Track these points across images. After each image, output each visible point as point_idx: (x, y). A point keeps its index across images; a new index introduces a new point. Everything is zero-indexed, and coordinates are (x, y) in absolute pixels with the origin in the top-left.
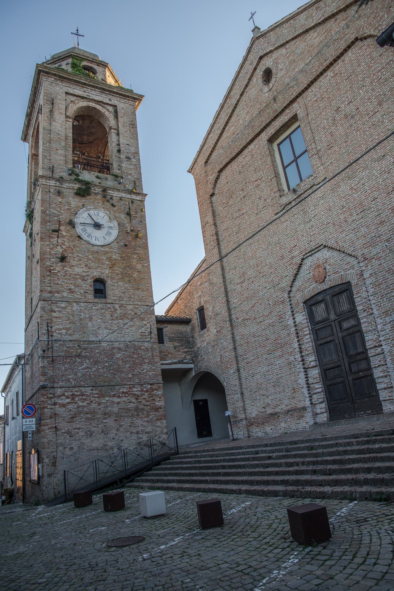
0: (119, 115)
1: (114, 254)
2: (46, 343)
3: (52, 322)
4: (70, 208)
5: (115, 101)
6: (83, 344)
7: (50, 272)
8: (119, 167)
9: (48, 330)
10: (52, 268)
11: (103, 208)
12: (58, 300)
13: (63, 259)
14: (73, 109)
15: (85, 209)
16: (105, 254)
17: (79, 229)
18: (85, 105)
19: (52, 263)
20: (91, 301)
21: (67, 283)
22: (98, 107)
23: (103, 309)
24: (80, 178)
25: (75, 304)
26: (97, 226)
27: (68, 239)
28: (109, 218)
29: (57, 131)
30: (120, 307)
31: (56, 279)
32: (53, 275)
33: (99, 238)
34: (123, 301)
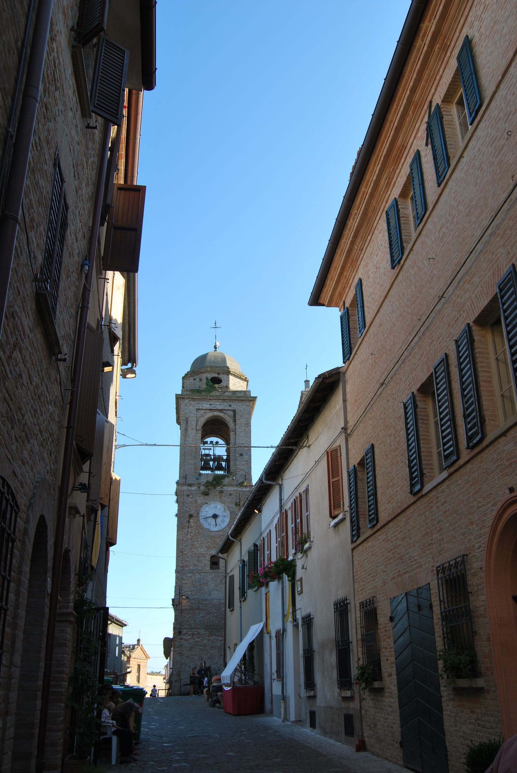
14: (202, 421)
22: (221, 414)
25: (197, 574)
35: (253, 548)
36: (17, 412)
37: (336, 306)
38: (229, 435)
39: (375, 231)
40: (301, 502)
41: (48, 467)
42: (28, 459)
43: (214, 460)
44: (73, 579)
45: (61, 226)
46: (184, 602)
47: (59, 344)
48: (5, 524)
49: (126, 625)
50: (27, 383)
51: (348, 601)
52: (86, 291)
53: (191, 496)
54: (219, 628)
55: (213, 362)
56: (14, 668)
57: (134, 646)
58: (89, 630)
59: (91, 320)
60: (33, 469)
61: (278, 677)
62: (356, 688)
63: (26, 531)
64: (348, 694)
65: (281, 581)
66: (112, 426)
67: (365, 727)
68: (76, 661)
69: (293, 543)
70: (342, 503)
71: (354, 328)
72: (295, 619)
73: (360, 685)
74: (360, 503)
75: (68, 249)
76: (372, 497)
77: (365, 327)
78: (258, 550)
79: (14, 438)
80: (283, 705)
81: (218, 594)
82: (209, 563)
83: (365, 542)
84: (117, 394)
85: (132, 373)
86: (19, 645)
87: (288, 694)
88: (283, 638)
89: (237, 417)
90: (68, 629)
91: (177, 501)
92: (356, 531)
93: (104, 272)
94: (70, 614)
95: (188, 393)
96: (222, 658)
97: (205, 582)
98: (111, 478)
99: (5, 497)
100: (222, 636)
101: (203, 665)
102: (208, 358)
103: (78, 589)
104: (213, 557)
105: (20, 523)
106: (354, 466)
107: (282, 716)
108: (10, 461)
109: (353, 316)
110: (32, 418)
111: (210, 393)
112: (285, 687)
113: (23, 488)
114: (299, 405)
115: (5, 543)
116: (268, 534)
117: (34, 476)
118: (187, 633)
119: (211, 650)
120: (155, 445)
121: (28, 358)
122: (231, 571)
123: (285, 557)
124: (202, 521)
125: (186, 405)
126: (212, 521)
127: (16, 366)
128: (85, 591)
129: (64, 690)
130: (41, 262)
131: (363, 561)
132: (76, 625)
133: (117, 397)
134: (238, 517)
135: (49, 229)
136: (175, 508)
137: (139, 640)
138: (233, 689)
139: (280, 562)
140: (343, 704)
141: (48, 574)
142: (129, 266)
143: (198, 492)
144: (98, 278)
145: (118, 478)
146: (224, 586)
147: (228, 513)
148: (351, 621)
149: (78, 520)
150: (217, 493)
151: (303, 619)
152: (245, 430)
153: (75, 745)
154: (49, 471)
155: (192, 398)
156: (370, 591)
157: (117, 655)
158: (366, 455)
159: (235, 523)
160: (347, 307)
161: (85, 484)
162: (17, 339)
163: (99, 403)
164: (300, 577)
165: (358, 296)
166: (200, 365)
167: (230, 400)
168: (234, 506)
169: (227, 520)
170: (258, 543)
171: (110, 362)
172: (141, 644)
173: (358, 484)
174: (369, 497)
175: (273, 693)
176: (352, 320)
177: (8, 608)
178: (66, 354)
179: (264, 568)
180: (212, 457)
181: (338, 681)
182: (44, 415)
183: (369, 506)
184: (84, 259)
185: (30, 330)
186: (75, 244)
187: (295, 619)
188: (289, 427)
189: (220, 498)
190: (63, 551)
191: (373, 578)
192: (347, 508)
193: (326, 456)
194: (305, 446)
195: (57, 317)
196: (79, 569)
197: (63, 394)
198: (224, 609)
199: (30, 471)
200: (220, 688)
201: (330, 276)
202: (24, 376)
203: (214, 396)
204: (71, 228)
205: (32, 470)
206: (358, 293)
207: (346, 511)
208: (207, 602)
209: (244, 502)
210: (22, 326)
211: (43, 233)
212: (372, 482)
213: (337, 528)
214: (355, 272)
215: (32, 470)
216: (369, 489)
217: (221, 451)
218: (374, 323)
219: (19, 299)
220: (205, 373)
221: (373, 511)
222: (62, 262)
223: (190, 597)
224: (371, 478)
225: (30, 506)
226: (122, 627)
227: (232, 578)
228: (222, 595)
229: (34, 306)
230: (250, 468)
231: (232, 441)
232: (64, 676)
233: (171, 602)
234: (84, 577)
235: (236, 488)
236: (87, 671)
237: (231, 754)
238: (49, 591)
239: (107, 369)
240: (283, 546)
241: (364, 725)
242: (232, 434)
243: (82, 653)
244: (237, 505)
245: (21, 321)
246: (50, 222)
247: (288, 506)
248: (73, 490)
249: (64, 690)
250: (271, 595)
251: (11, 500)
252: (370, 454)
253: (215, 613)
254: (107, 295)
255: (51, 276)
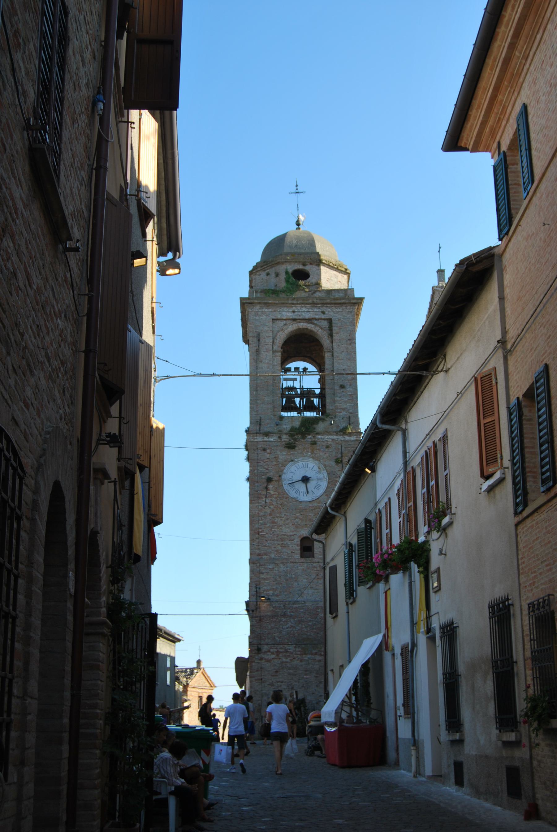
22: (310, 326)
25: (282, 565)
35: (363, 526)
36: (13, 330)
37: (486, 150)
38: (323, 358)
39: (549, 26)
40: (436, 456)
41: (61, 411)
42: (33, 400)
43: (301, 396)
44: (104, 573)
45: (60, 42)
46: (264, 606)
47: (68, 226)
48: (6, 494)
49: (179, 640)
50: (25, 286)
51: (510, 602)
52: (102, 142)
53: (268, 451)
54: (316, 643)
55: (296, 246)
56: (29, 700)
57: (192, 670)
58: (130, 647)
59: (112, 188)
60: (42, 413)
61: (406, 712)
62: (524, 729)
63: (35, 505)
64: (512, 737)
65: (407, 573)
66: (149, 349)
67: (537, 784)
68: (113, 690)
69: (424, 516)
70: (499, 456)
71: (515, 184)
72: (429, 630)
73: (530, 725)
74: (527, 455)
75: (71, 78)
76: (546, 445)
77: (533, 182)
78: (371, 528)
79: (10, 368)
80: (413, 753)
81: (313, 594)
82: (299, 548)
83: (536, 514)
84: (154, 300)
85: (174, 268)
86: (34, 667)
87: (421, 738)
88: (412, 656)
89: (335, 329)
90: (101, 645)
91: (248, 459)
92: (522, 498)
93: (126, 111)
94: (103, 623)
95: (259, 295)
96: (322, 685)
97: (294, 576)
98: (152, 427)
99: (5, 455)
100: (321, 655)
101: (295, 696)
102: (288, 240)
103: (112, 588)
104: (304, 540)
105: (28, 495)
106: (518, 398)
107: (414, 769)
108: (8, 404)
109: (513, 164)
110: (35, 338)
111: (292, 294)
112: (417, 729)
113: (27, 442)
114: (430, 309)
115: (8, 522)
116: (386, 503)
117: (42, 424)
118: (269, 651)
119: (306, 675)
120: (214, 375)
121: (23, 248)
122: (332, 560)
123: (413, 538)
124: (286, 487)
125: (257, 314)
126: (301, 487)
127: (8, 260)
128: (121, 590)
129: (99, 731)
130: (33, 101)
131: (534, 541)
132: (111, 639)
133: (154, 305)
134: (341, 480)
135: (41, 48)
136: (245, 468)
137: (199, 662)
138: (339, 730)
139: (406, 546)
140: (504, 753)
141: (69, 566)
142: (163, 100)
143: (279, 444)
144: (118, 122)
145: (161, 426)
146: (322, 581)
148: (515, 631)
149: (108, 488)
150: (308, 445)
151: (442, 628)
152: (347, 349)
153: (118, 808)
154: (63, 415)
155: (266, 303)
156: (544, 586)
157: (168, 683)
158: (537, 382)
159: (336, 488)
160: (504, 152)
161: (114, 434)
162: (6, 220)
163: (129, 314)
164: (437, 567)
165: (522, 132)
166: (276, 251)
168: (333, 463)
169: (324, 485)
170: (372, 518)
171: (142, 251)
172: (202, 666)
173: (524, 426)
174: (541, 445)
175: (400, 736)
176: (511, 172)
177: (17, 614)
178: (78, 241)
179: (382, 555)
180: (299, 390)
181: (496, 718)
182: (51, 333)
183: (542, 459)
184: (96, 92)
185: (24, 205)
186: (81, 69)
187: (429, 630)
188: (415, 341)
189: (312, 452)
190: (89, 533)
191: (548, 568)
192: (507, 463)
193: (474, 384)
194: (441, 371)
195: (61, 183)
196: (112, 559)
197: (77, 302)
198: (322, 615)
199: (36, 417)
200: (320, 729)
201: (476, 103)
202: (19, 276)
203: (298, 299)
204: (74, 45)
205: (39, 416)
206: (521, 127)
207: (505, 468)
208: (297, 606)
209: (349, 458)
210: (13, 200)
211: (34, 53)
212: (545, 423)
213: (492, 493)
214: (516, 94)
215: (39, 416)
216: (541, 434)
217: (311, 382)
218: (547, 174)
219: (5, 157)
220: (283, 263)
221: (548, 467)
222: (63, 98)
223: (273, 598)
224: (544, 416)
225: (39, 468)
226: (174, 642)
227: (334, 570)
228: (319, 595)
229: (27, 168)
230: (356, 406)
231: (328, 366)
232: (98, 711)
233: (244, 607)
234: (120, 570)
235: (335, 437)
236: (131, 704)
237: (340, 821)
238: (72, 591)
239: (138, 262)
240: (409, 521)
241: (535, 781)
242: (327, 355)
243: (122, 679)
244: (338, 461)
245: (11, 192)
246: (43, 35)
247: (416, 462)
248: (98, 444)
249: (99, 731)
250: (393, 594)
251: (12, 460)
252: (542, 380)
253: (310, 621)
254: (132, 149)
255: (49, 121)
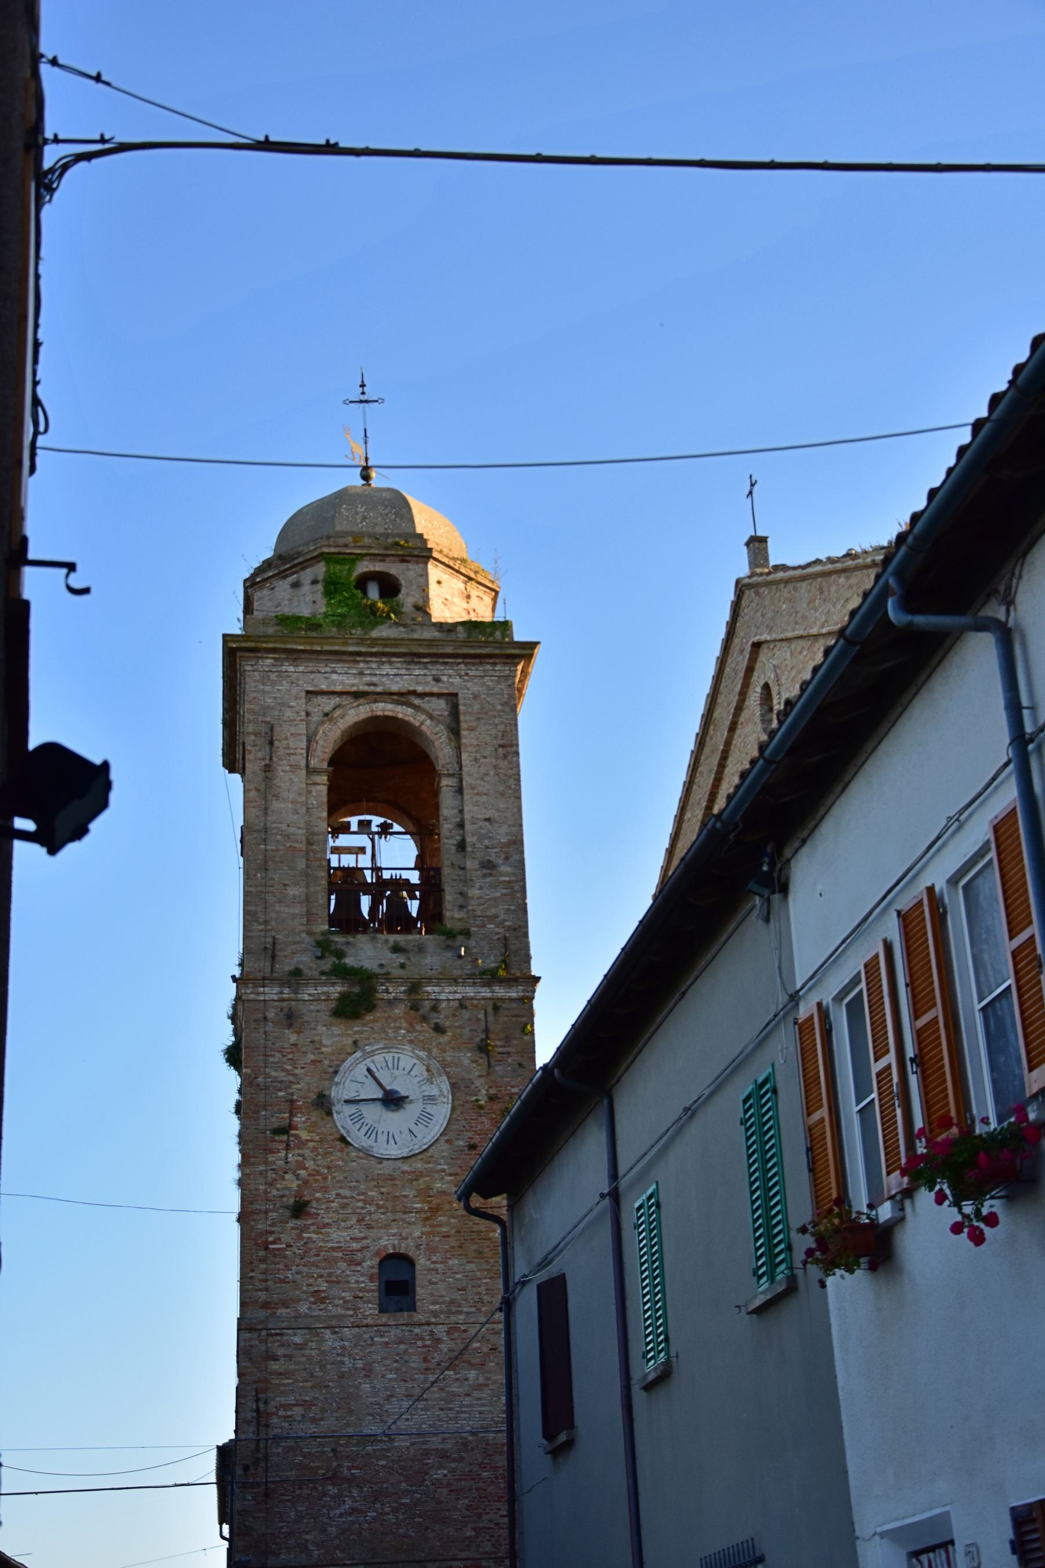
0: (463, 725)
1: (436, 1176)
2: (253, 1445)
3: (267, 1389)
4: (319, 1057)
5: (452, 678)
6: (346, 1445)
7: (266, 1248)
8: (461, 901)
9: (257, 1411)
10: (271, 1239)
11: (411, 1042)
12: (285, 1324)
13: (299, 1209)
14: (328, 739)
15: (358, 1054)
16: (412, 1181)
17: (343, 1117)
18: (363, 716)
19: (273, 1225)
20: (369, 1321)
21: (309, 1276)
22: (402, 712)
23: (400, 1342)
24: (349, 961)
25: (328, 1334)
26: (393, 1101)
27: (315, 1149)
28: (428, 1070)
29: (284, 827)
30: (448, 1333)
31: (281, 1266)
32: (275, 1256)
33: (395, 1136)
34: (460, 1313)
82: (374, 1285)
125: (265, 679)
147: (444, 1084)
152: (496, 767)
167: (437, 657)
217: (399, 854)
253: (406, 1492)
